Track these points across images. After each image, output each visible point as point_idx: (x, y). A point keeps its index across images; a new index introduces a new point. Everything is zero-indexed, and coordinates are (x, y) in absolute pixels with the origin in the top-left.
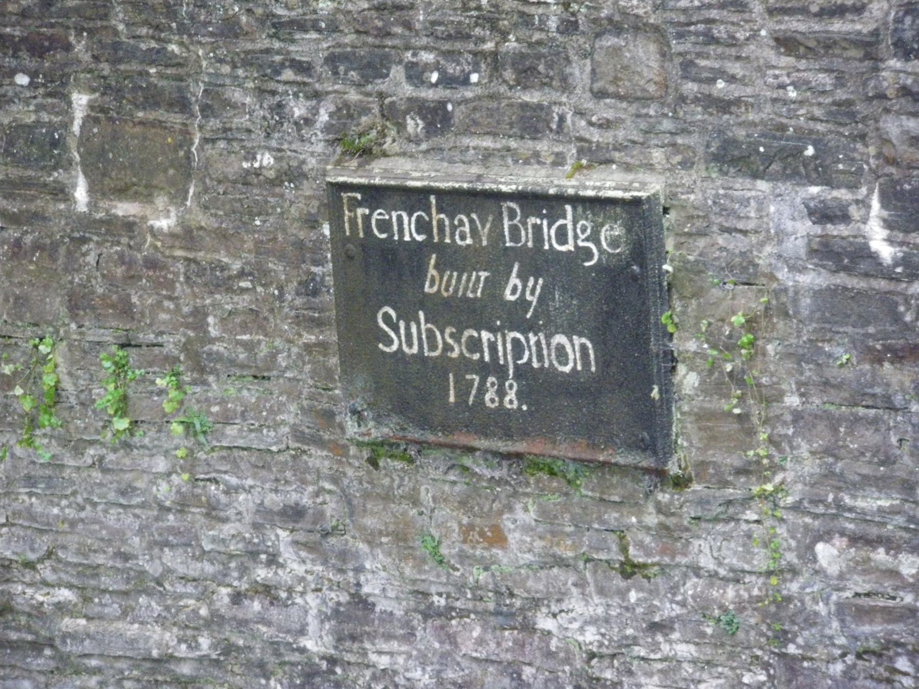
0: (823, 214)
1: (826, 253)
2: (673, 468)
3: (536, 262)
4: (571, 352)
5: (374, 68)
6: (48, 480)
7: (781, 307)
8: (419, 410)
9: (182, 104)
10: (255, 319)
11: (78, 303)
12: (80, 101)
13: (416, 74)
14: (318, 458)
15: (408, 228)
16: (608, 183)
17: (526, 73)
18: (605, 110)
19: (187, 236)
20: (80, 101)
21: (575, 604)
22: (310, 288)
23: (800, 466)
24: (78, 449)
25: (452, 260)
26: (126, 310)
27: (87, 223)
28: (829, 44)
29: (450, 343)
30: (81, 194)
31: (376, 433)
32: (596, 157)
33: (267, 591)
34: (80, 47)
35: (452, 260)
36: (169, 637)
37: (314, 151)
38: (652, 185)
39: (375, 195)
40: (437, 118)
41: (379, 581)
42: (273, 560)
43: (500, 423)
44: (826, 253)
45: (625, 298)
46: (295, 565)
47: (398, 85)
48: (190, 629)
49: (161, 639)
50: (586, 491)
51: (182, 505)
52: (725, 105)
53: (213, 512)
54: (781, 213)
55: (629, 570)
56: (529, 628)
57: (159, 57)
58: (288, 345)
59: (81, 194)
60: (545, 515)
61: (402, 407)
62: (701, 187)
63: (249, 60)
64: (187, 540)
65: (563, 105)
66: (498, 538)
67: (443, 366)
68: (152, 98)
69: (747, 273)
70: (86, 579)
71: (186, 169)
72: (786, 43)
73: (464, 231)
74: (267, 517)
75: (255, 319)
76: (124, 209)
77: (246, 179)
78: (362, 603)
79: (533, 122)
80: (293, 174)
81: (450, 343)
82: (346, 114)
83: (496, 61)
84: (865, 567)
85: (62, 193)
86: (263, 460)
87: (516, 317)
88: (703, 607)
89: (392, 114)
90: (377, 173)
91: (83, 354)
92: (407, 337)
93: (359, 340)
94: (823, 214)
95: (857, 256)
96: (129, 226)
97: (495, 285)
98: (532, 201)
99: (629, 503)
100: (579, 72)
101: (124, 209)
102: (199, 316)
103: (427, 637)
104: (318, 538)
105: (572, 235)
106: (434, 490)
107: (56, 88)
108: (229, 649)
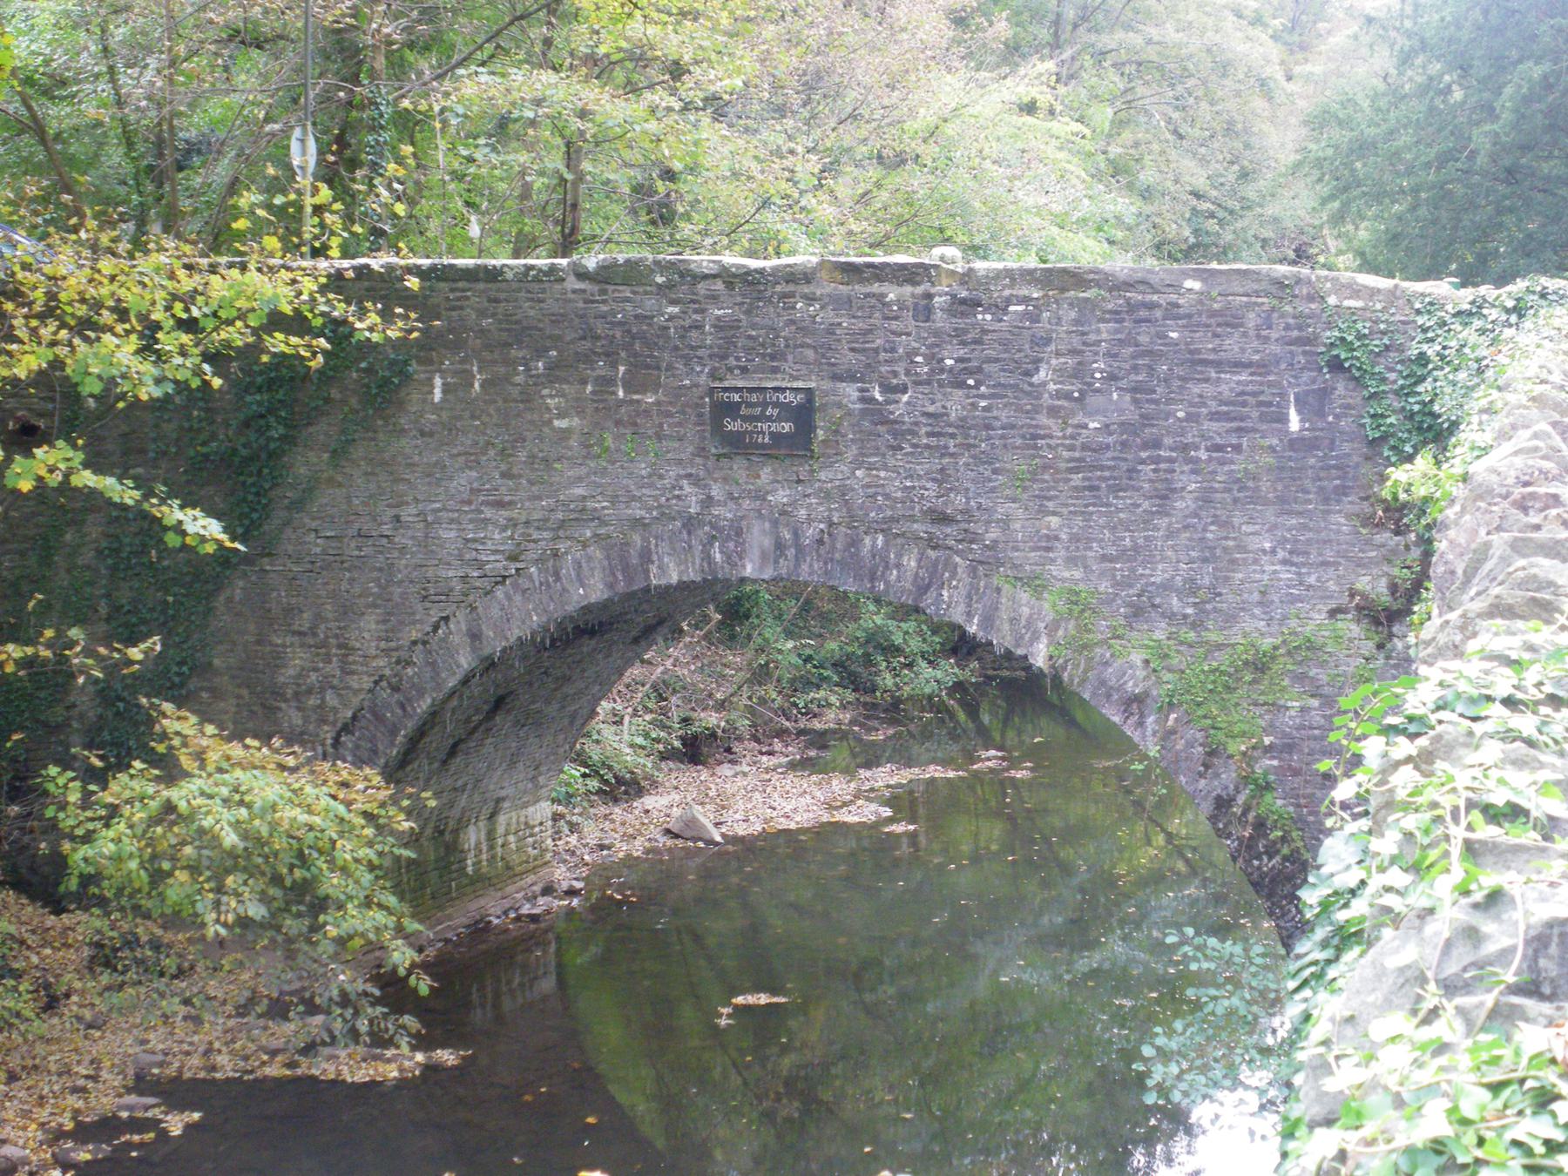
0: (862, 390)
1: (862, 400)
2: (420, 646)
3: (776, 405)
4: (787, 427)
5: (724, 357)
6: (604, 472)
7: (849, 413)
8: (738, 445)
9: (658, 368)
10: (680, 424)
11: (618, 423)
12: (622, 369)
13: (738, 359)
14: (698, 460)
15: (737, 398)
16: (800, 384)
17: (773, 357)
18: (797, 367)
19: (658, 403)
20: (622, 369)
21: (781, 492)
22: (700, 415)
23: (854, 450)
24: (613, 463)
25: (750, 405)
26: (635, 424)
27: (623, 401)
28: (864, 350)
29: (748, 426)
30: (621, 394)
31: (721, 451)
32: (796, 378)
33: (678, 497)
34: (623, 354)
35: (750, 405)
36: (643, 513)
37: (703, 379)
38: (813, 385)
39: (726, 389)
40: (744, 370)
41: (716, 491)
42: (681, 488)
43: (763, 446)
44: (862, 400)
45: (804, 414)
46: (688, 489)
47: (732, 362)
48: (650, 510)
49: (639, 513)
50: (787, 462)
51: (650, 476)
52: (834, 365)
53: (661, 477)
54: (851, 391)
55: (799, 481)
56: (765, 499)
57: (651, 356)
58: (690, 431)
59: (621, 394)
60: (774, 470)
61: (731, 444)
62: (826, 385)
63: (682, 357)
64: (651, 485)
65: (785, 366)
66: (759, 477)
67: (746, 432)
68: (648, 367)
69: (839, 405)
70: (614, 500)
71: (659, 385)
72: (852, 350)
73: (754, 398)
74: (679, 477)
75: (680, 424)
76: (636, 397)
77: (680, 387)
78: (710, 498)
79: (775, 370)
80: (697, 386)
81: (748, 426)
82: (714, 369)
83: (763, 356)
84: (869, 475)
85: (614, 393)
86: (680, 462)
87: (769, 419)
88: (821, 490)
89: (730, 370)
90: (726, 384)
91: (617, 438)
92: (732, 426)
93: (717, 427)
94: (862, 390)
95: (872, 400)
96: (638, 401)
97: (763, 412)
98: (776, 389)
99: (801, 465)
100: (790, 357)
101: (636, 397)
102: (661, 425)
103: (731, 505)
104: (696, 481)
105: (789, 397)
106: (739, 467)
107: (614, 366)
108: (663, 514)
